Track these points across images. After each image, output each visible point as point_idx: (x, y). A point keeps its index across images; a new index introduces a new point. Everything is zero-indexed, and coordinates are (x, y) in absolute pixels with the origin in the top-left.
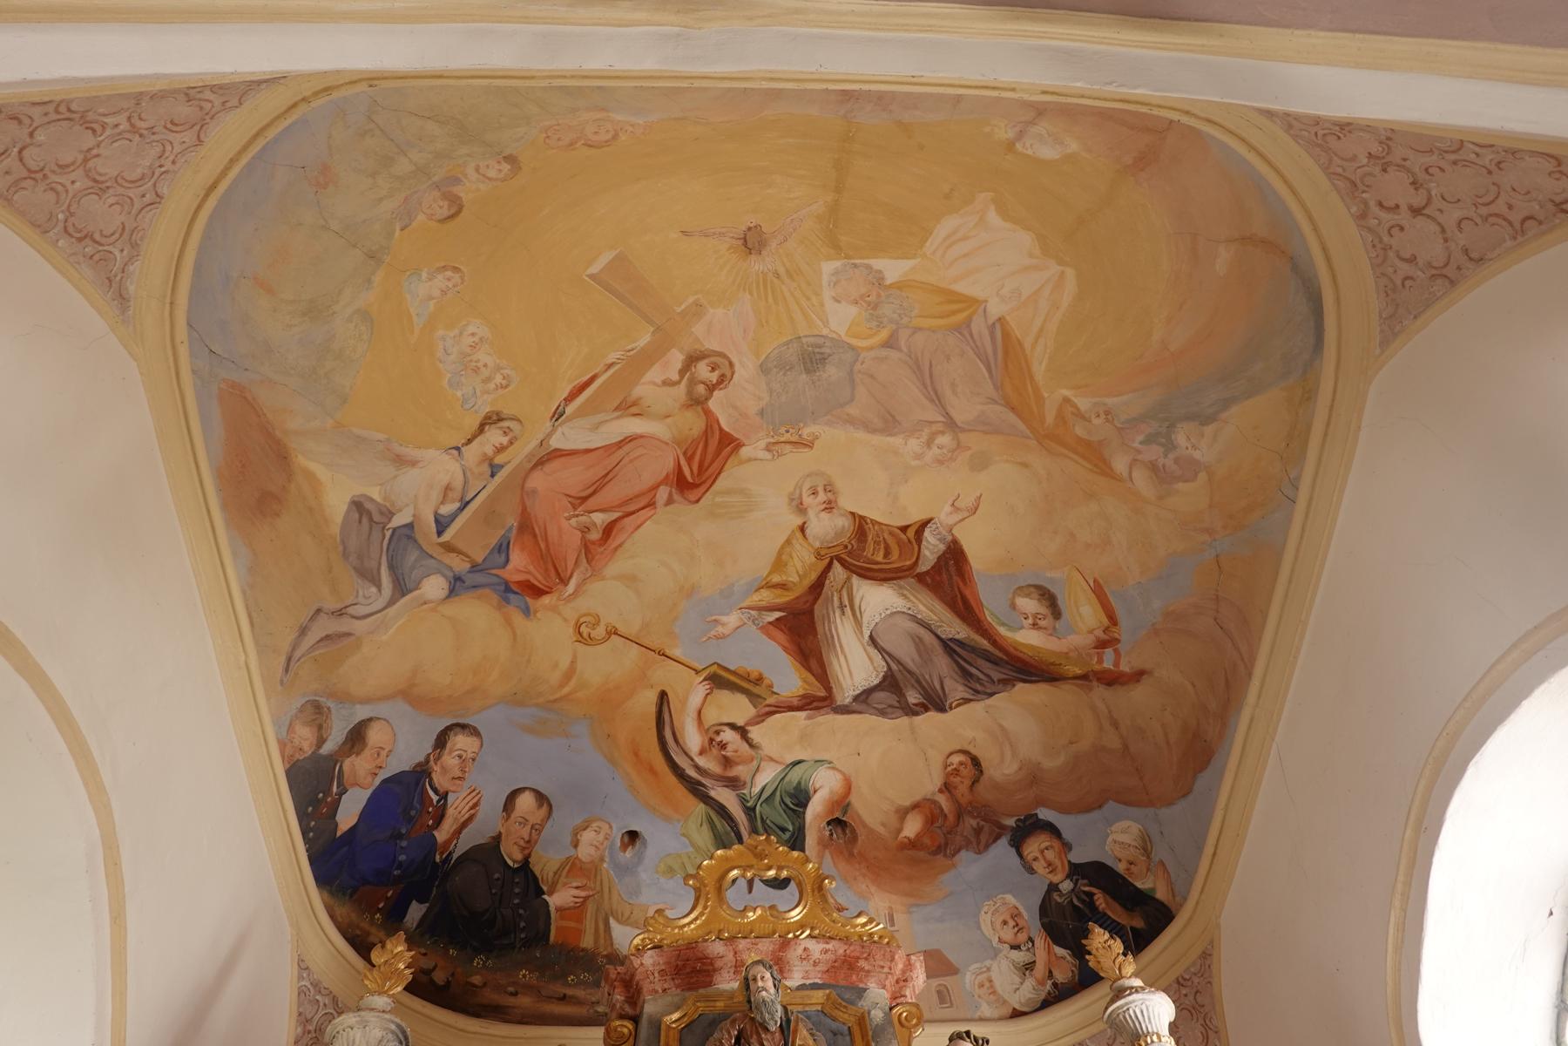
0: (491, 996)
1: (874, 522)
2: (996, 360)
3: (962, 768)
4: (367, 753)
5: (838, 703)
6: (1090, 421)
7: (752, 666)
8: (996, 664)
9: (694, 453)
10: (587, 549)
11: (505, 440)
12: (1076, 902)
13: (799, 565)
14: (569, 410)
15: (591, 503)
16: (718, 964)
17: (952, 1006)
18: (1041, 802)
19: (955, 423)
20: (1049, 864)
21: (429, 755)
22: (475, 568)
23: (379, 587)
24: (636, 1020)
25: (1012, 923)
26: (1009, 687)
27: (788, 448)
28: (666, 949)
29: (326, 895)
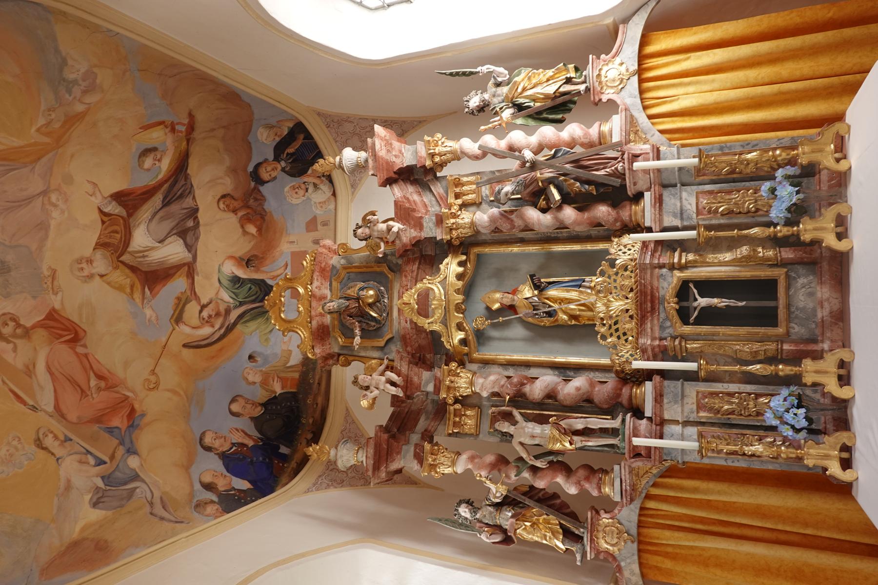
0: (317, 414)
1: (99, 238)
2: (8, 165)
3: (226, 203)
4: (216, 481)
5: (191, 260)
6: (53, 119)
7: (172, 302)
8: (177, 181)
9: (57, 334)
10: (109, 388)
11: (51, 436)
12: (290, 161)
13: (122, 278)
14: (31, 403)
15: (85, 387)
16: (320, 323)
17: (329, 221)
18: (245, 170)
19: (45, 190)
20: (273, 170)
21: (215, 454)
22: (122, 443)
23: (136, 488)
24: (339, 355)
25: (297, 190)
26: (189, 177)
27: (55, 283)
28: (314, 344)
29: (278, 488)
